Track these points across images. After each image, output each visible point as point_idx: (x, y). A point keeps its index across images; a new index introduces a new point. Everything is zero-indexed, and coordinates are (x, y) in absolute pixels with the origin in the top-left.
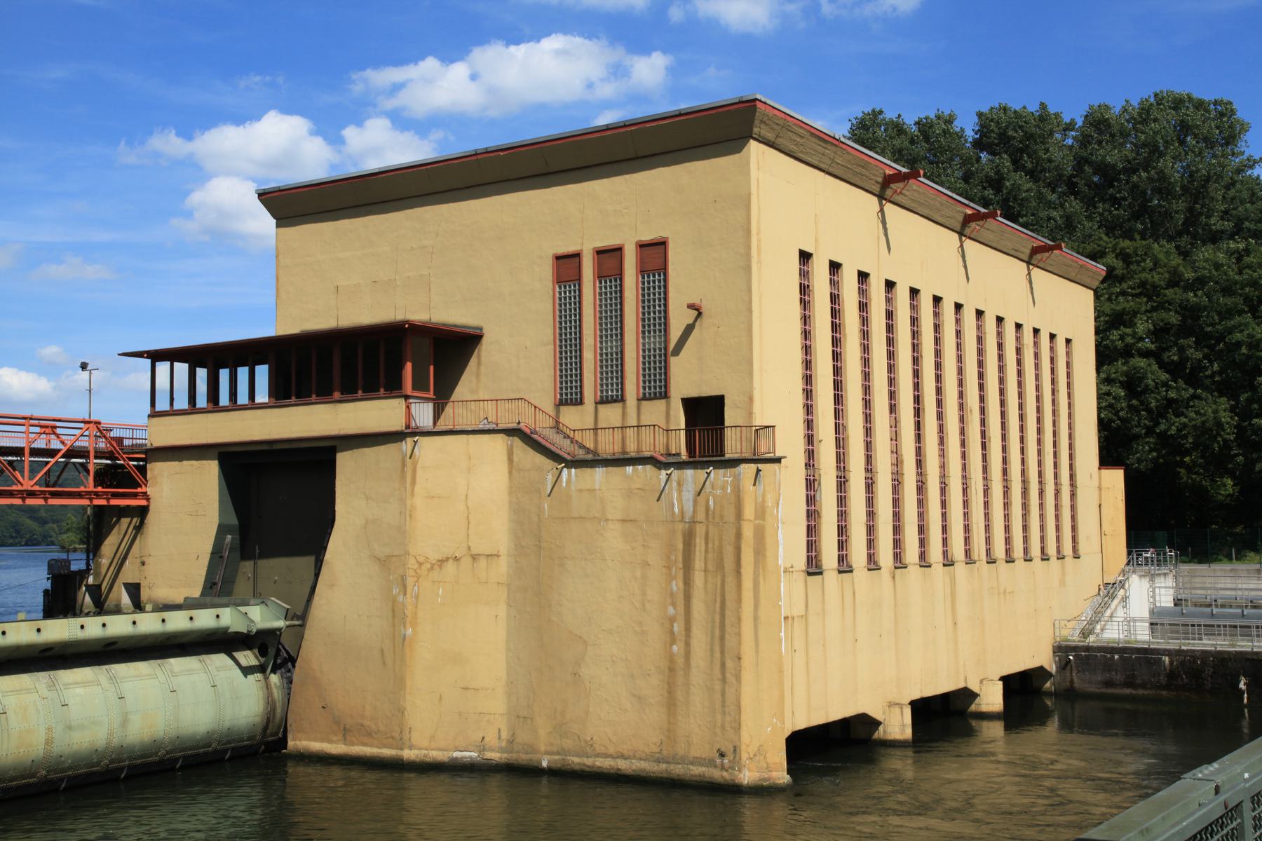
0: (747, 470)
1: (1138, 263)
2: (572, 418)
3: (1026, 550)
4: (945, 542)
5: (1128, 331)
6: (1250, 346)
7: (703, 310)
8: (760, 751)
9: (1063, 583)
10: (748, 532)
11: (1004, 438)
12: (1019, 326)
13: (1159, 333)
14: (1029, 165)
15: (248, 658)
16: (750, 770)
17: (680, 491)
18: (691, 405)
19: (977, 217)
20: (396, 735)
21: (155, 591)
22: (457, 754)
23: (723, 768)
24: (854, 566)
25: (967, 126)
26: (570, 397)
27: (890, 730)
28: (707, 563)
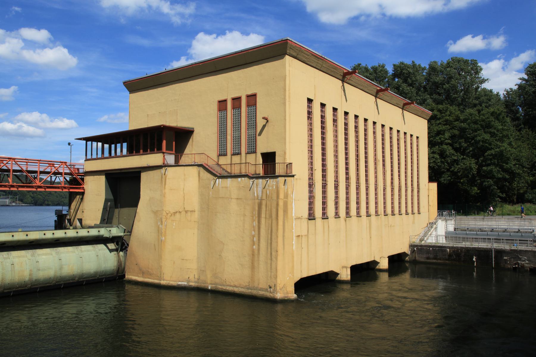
0: (281, 180)
1: (444, 113)
2: (223, 161)
3: (400, 211)
4: (367, 208)
5: (443, 136)
6: (483, 141)
7: (269, 119)
8: (284, 286)
9: (414, 223)
10: (281, 203)
11: (392, 171)
13: (453, 137)
14: (410, 82)
15: (112, 246)
16: (280, 293)
17: (257, 188)
18: (264, 155)
19: (381, 90)
20: (159, 275)
21: (87, 222)
22: (180, 283)
23: (270, 292)
24: (329, 217)
25: (390, 70)
26: (222, 153)
27: (342, 276)
28: (266, 215)
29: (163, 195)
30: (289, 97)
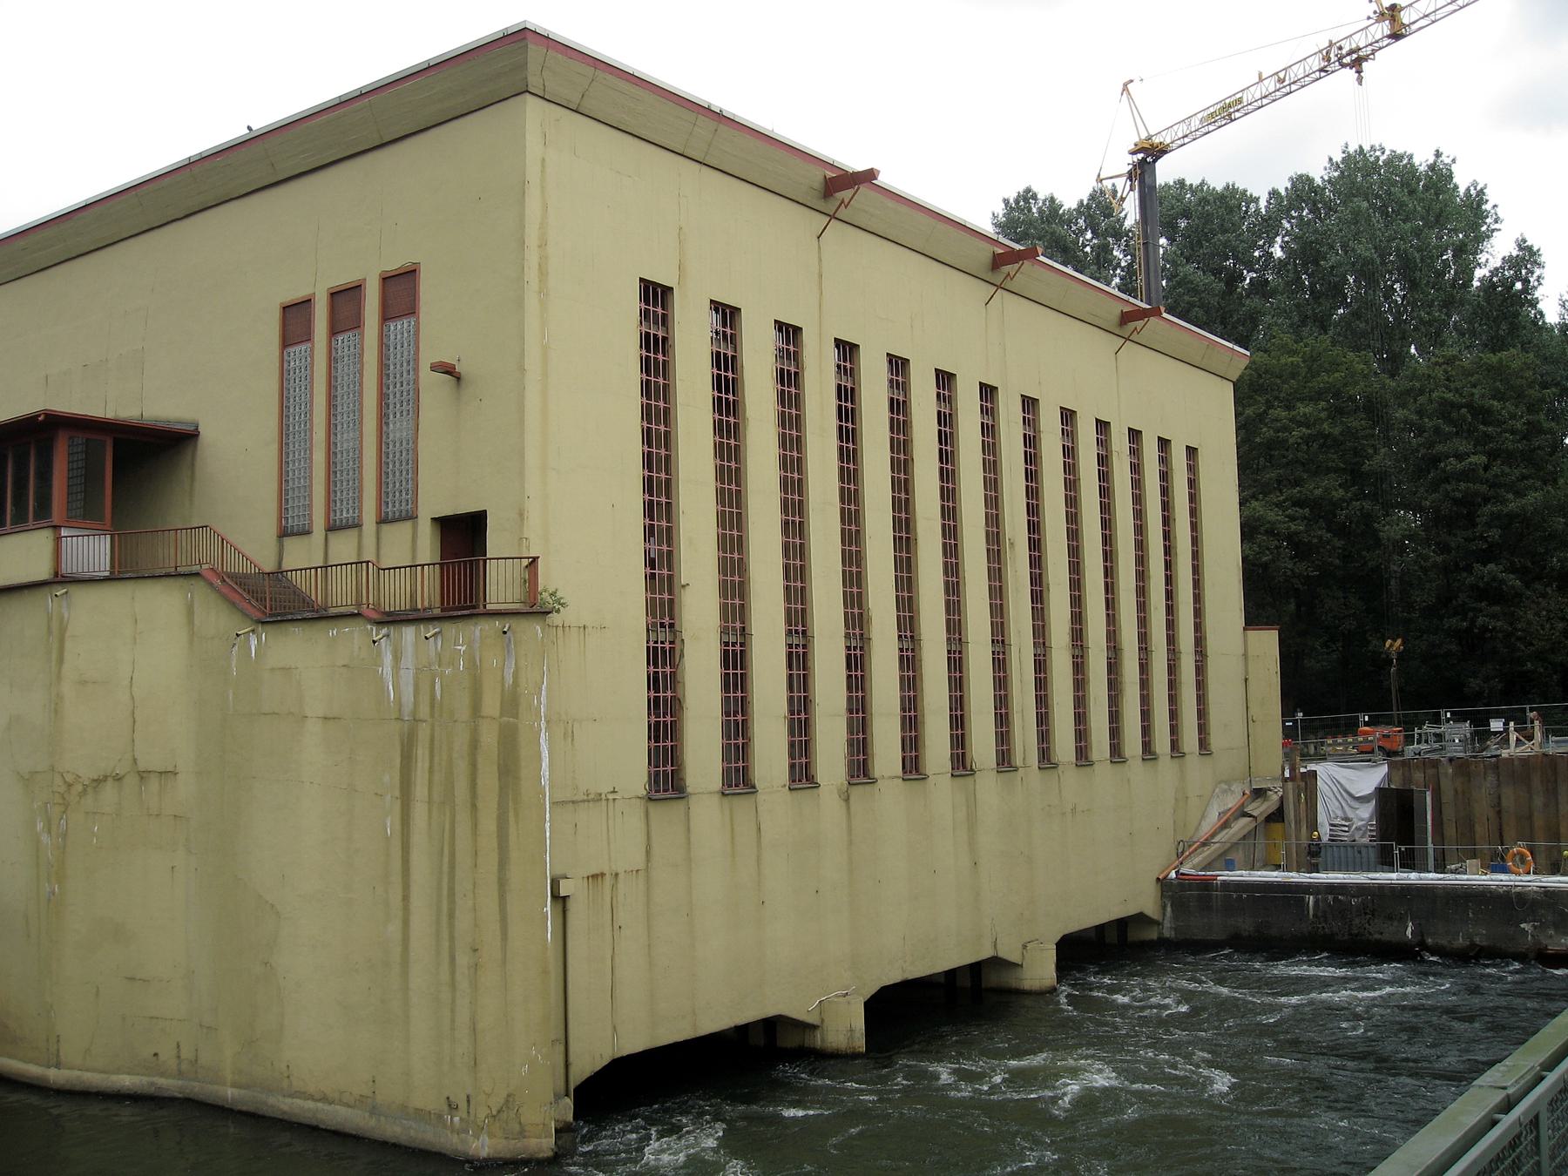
2: (301, 555)
12: (1029, 404)
16: (491, 1135)
19: (1140, 314)
29: (56, 708)
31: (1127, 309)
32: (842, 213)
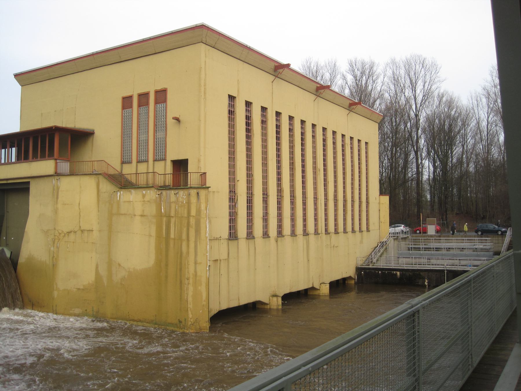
0: (193, 192)
8: (196, 321)
9: (361, 242)
10: (192, 221)
12: (303, 122)
29: (56, 211)
30: (205, 93)
31: (351, 102)
32: (353, 110)
